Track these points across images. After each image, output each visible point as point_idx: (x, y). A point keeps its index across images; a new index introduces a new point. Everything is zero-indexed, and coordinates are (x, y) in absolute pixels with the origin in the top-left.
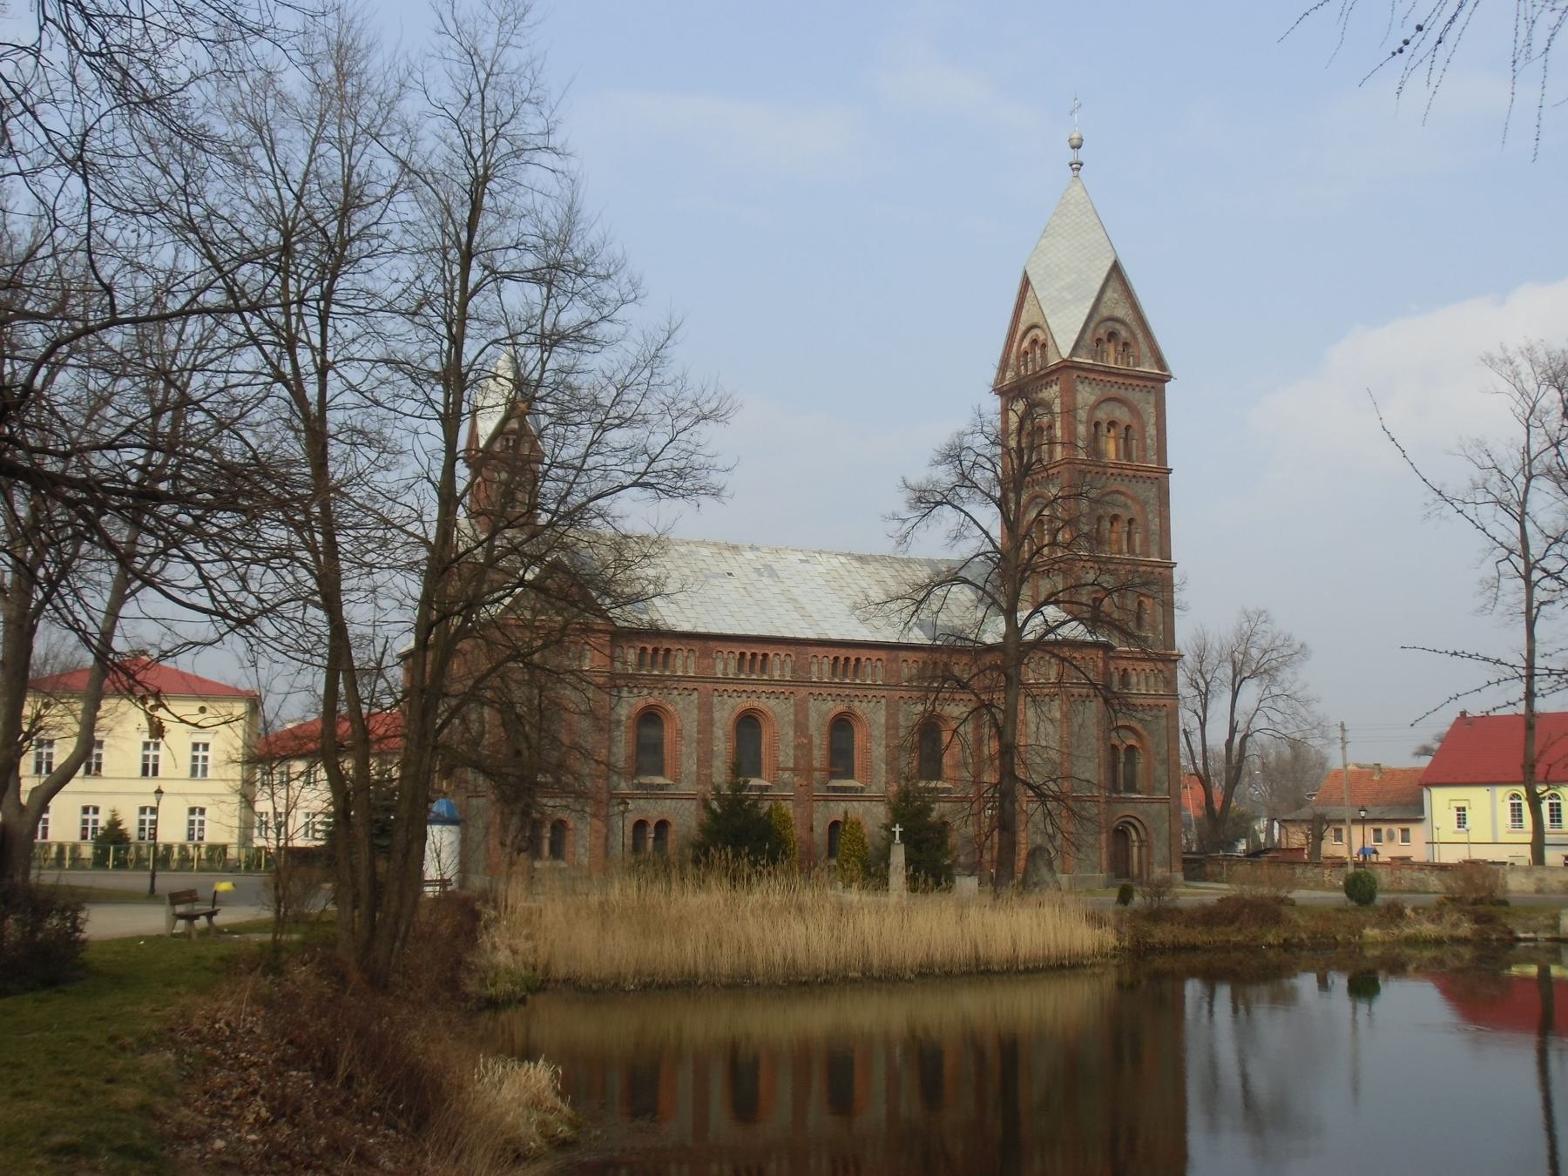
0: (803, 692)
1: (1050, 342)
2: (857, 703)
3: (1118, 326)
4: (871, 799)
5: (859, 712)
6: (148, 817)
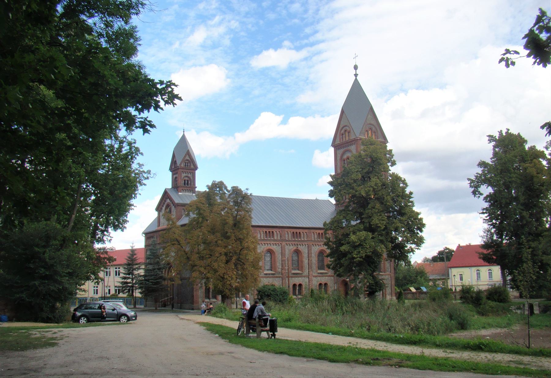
0: (284, 243)
1: (352, 131)
2: (299, 246)
3: (372, 126)
4: (304, 277)
5: (300, 249)
6: (96, 288)
